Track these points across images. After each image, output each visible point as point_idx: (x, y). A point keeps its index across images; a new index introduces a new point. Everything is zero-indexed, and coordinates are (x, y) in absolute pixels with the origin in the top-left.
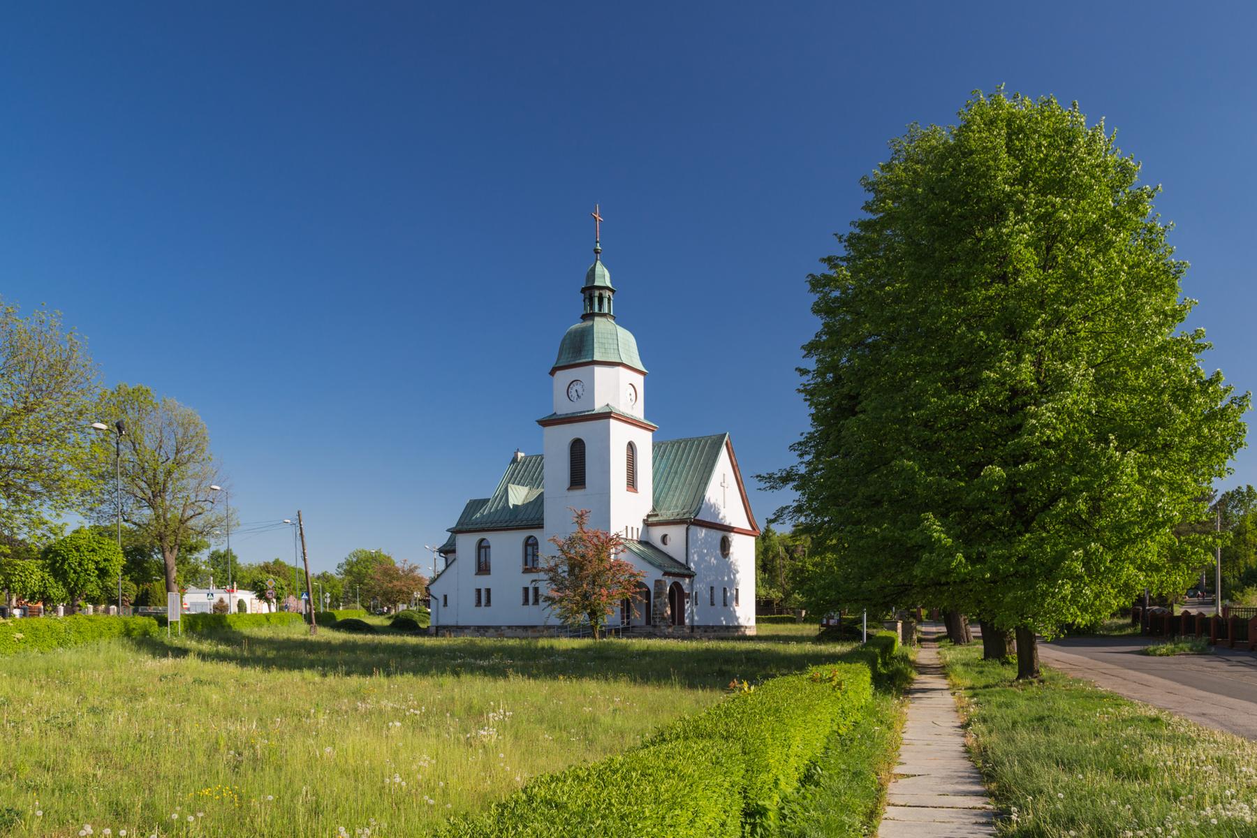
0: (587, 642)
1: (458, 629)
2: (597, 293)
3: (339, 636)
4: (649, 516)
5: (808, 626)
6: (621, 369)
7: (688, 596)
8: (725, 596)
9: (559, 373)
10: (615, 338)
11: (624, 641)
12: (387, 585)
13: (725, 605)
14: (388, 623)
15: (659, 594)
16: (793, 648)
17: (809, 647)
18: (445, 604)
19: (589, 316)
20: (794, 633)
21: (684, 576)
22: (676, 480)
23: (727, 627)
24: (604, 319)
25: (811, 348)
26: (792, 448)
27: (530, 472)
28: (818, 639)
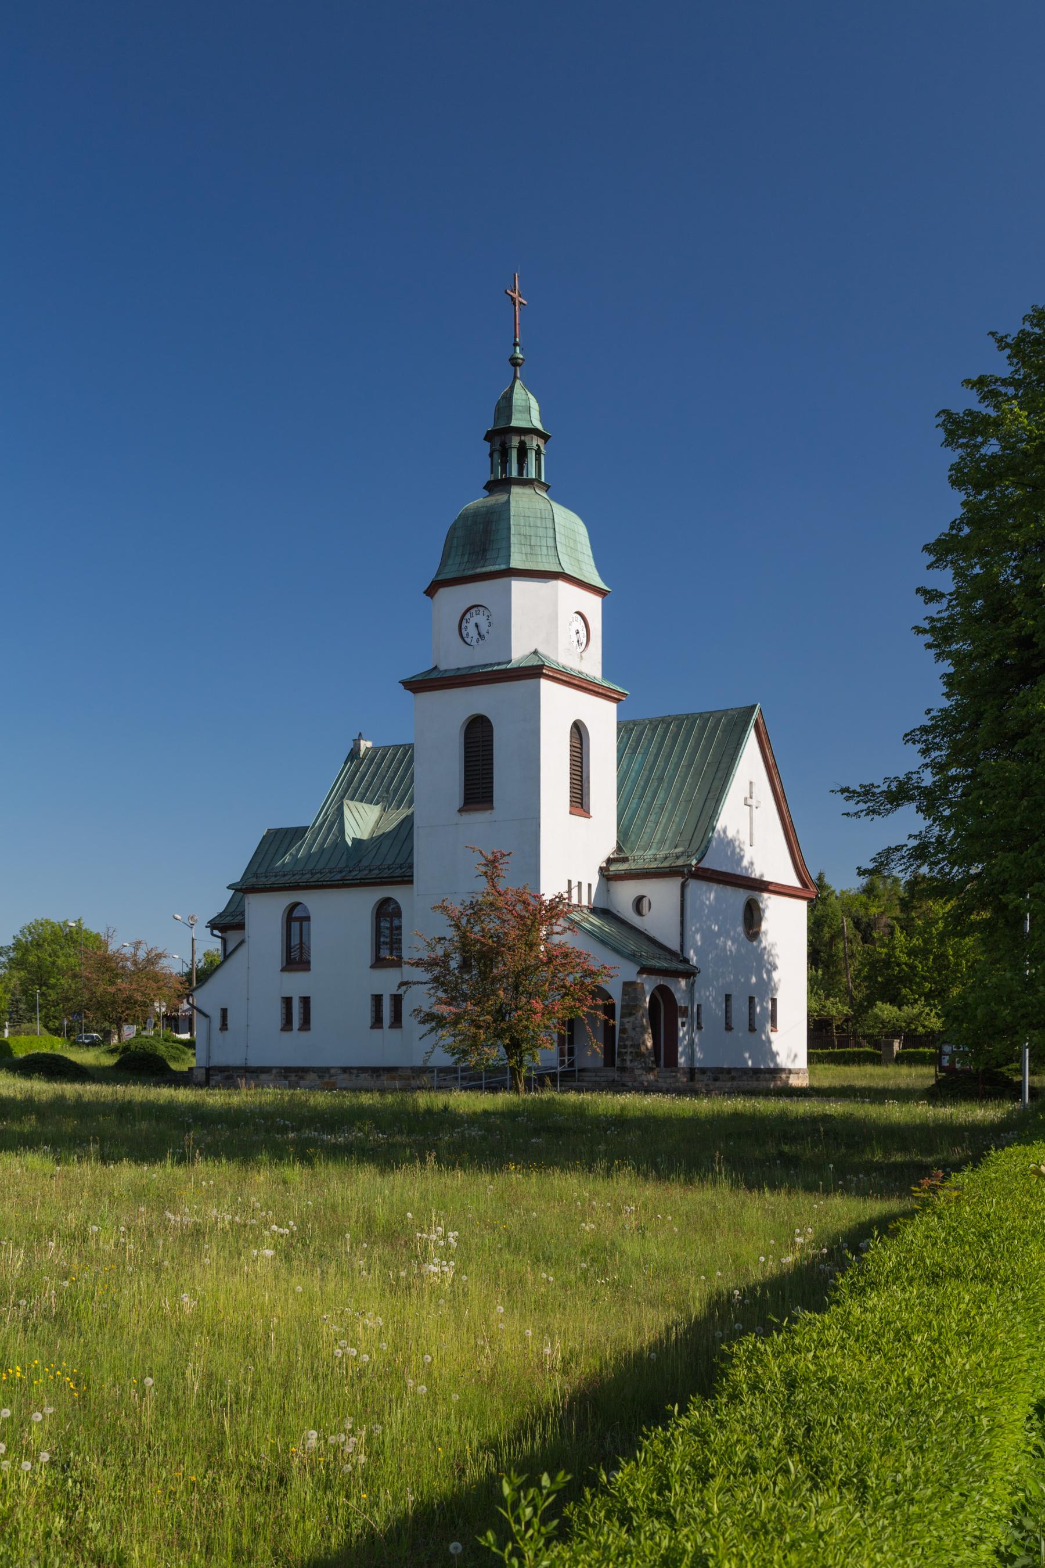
0: (502, 1100)
1: (254, 1073)
2: (515, 441)
3: (41, 1088)
4: (609, 861)
5: (904, 1070)
6: (561, 584)
7: (684, 1012)
8: (754, 1012)
9: (443, 593)
10: (550, 527)
11: (572, 1097)
12: (103, 988)
13: (752, 1029)
14: (109, 1061)
15: (630, 1009)
16: (895, 1112)
17: (923, 1111)
18: (224, 1026)
19: (500, 485)
20: (891, 1084)
21: (676, 974)
22: (661, 794)
23: (756, 1072)
24: (528, 491)
25: (943, 550)
26: (909, 738)
27: (382, 773)
28: (934, 1095)
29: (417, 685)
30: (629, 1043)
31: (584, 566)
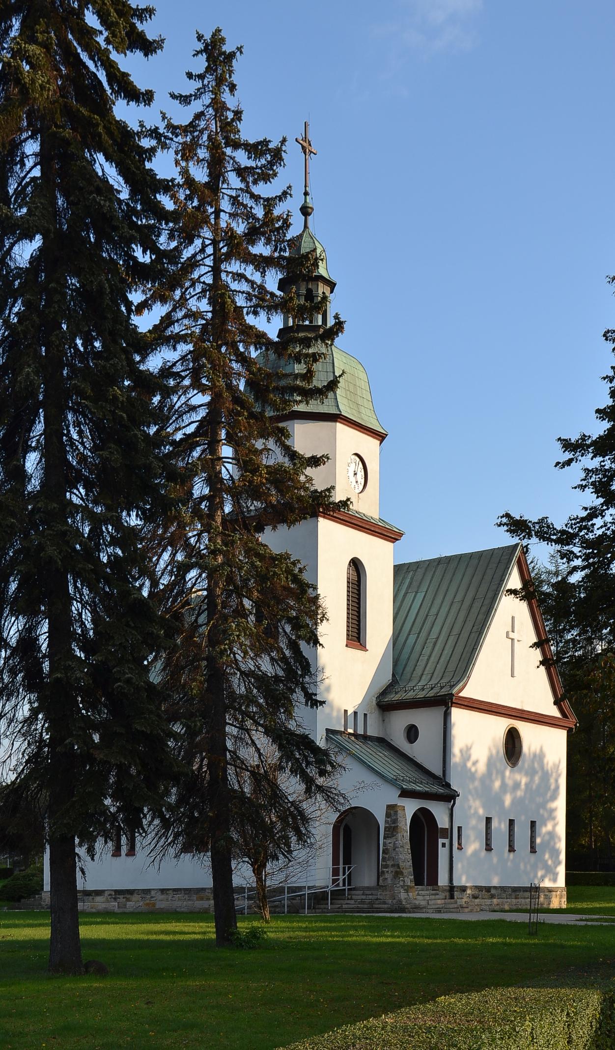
6: (339, 426)
10: (38, 242)
15: (392, 830)
29: (513, 618)
30: (390, 863)
31: (363, 410)
